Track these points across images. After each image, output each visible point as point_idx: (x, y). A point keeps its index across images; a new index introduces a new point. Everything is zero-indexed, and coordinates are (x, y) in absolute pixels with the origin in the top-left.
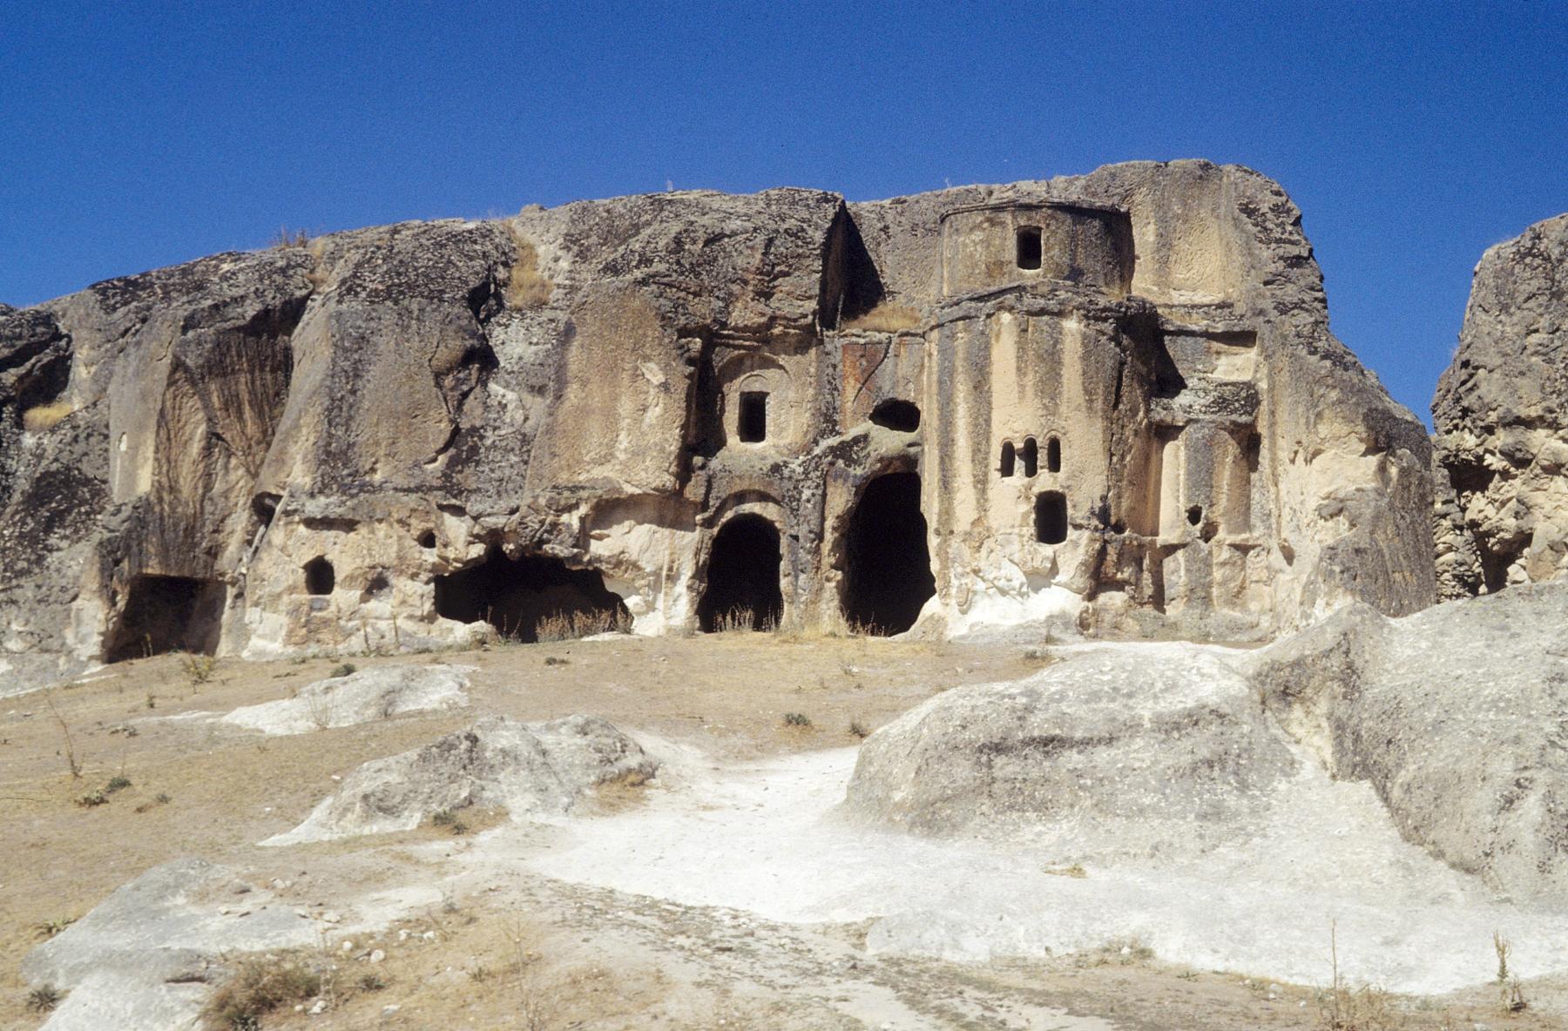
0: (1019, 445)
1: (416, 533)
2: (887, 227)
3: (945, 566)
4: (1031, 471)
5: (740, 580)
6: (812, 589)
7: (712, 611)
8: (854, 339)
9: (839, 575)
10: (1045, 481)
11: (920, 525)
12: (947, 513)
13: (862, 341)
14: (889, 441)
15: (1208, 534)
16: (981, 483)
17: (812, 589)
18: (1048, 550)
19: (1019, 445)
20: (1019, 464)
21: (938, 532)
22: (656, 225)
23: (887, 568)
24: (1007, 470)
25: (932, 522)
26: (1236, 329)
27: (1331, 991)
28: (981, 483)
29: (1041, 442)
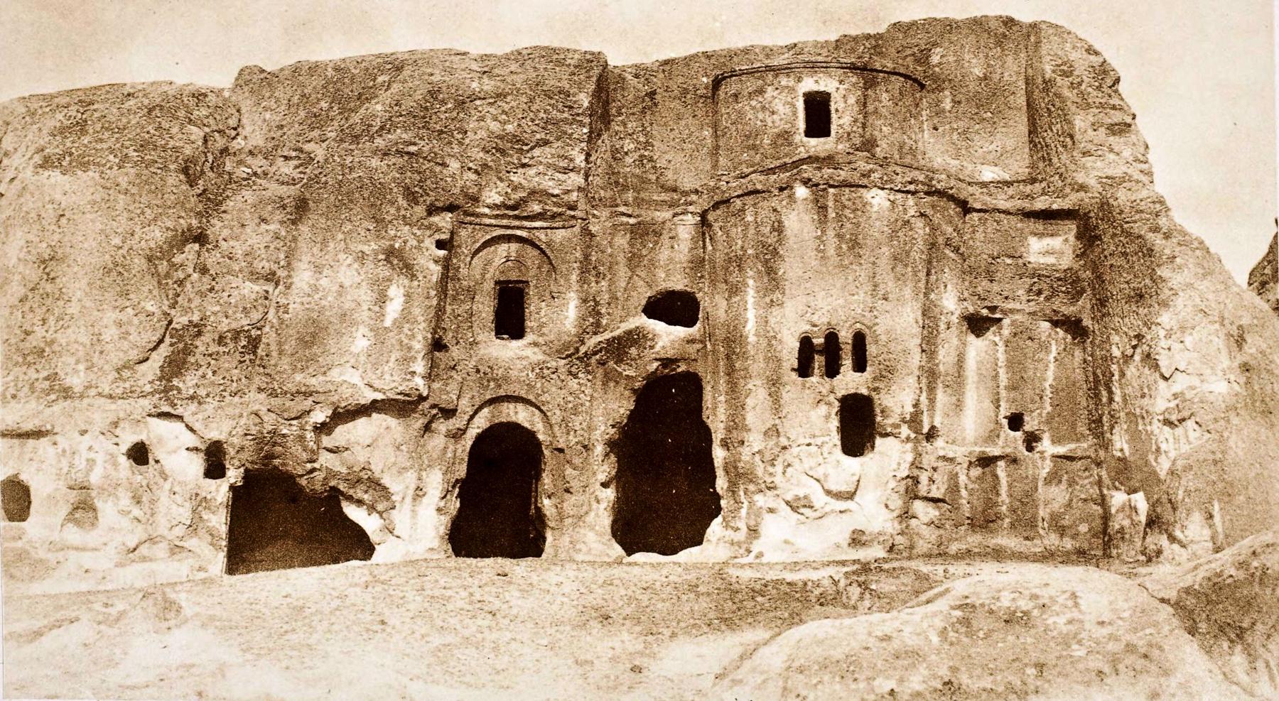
0: (818, 341)
1: (125, 447)
2: (654, 93)
3: (732, 490)
4: (832, 370)
5: (498, 506)
6: (583, 505)
7: (467, 538)
8: (625, 219)
9: (610, 494)
10: (850, 381)
11: (705, 435)
12: (736, 424)
13: (632, 221)
14: (667, 336)
15: (1031, 440)
16: (774, 383)
17: (583, 505)
18: (852, 463)
19: (818, 341)
20: (819, 361)
21: (725, 444)
22: (396, 87)
23: (671, 477)
24: (804, 369)
25: (718, 435)
26: (1055, 207)
27: (512, 53)
28: (774, 383)
29: (845, 336)
